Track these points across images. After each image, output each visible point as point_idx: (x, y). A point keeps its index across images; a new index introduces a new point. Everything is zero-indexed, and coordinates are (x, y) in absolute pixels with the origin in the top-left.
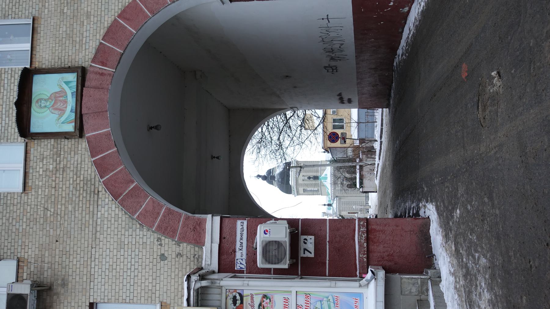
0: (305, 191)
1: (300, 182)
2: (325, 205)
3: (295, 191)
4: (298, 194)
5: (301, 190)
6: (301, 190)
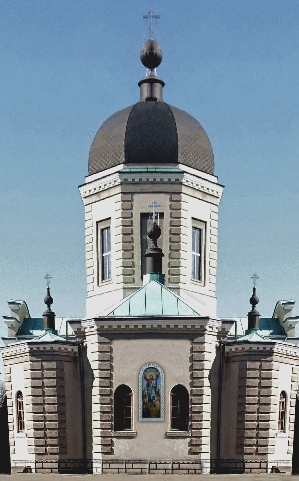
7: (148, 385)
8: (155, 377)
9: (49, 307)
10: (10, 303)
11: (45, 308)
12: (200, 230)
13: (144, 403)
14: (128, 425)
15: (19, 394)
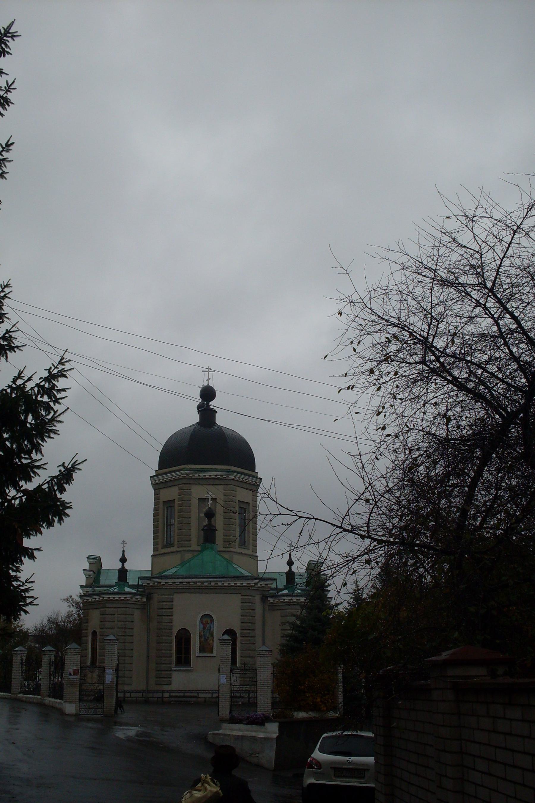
0: (169, 504)
1: (198, 491)
2: (123, 560)
3: (169, 476)
4: (159, 484)
5: (172, 493)
6: (172, 493)
7: (204, 628)
8: (209, 622)
9: (123, 565)
10: (84, 570)
11: (119, 566)
12: (245, 509)
13: (200, 642)
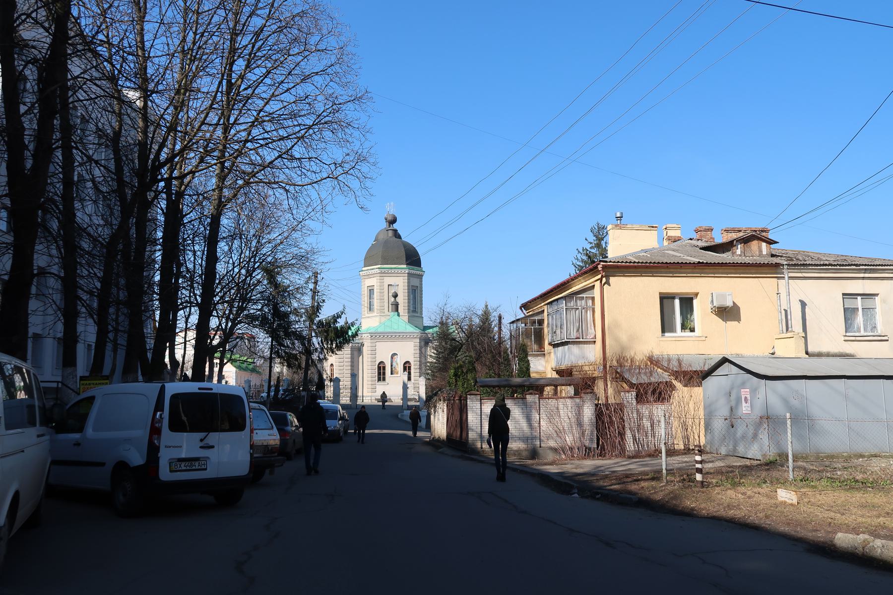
14: (384, 379)
15: (332, 365)
